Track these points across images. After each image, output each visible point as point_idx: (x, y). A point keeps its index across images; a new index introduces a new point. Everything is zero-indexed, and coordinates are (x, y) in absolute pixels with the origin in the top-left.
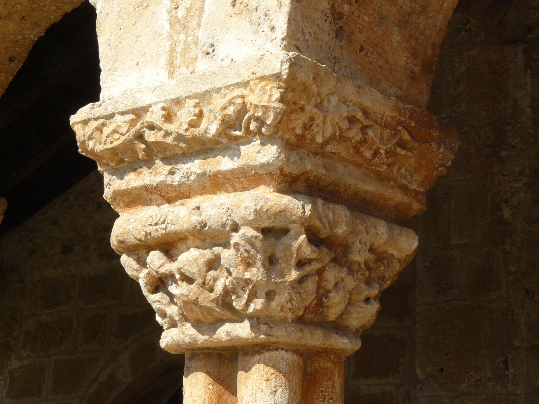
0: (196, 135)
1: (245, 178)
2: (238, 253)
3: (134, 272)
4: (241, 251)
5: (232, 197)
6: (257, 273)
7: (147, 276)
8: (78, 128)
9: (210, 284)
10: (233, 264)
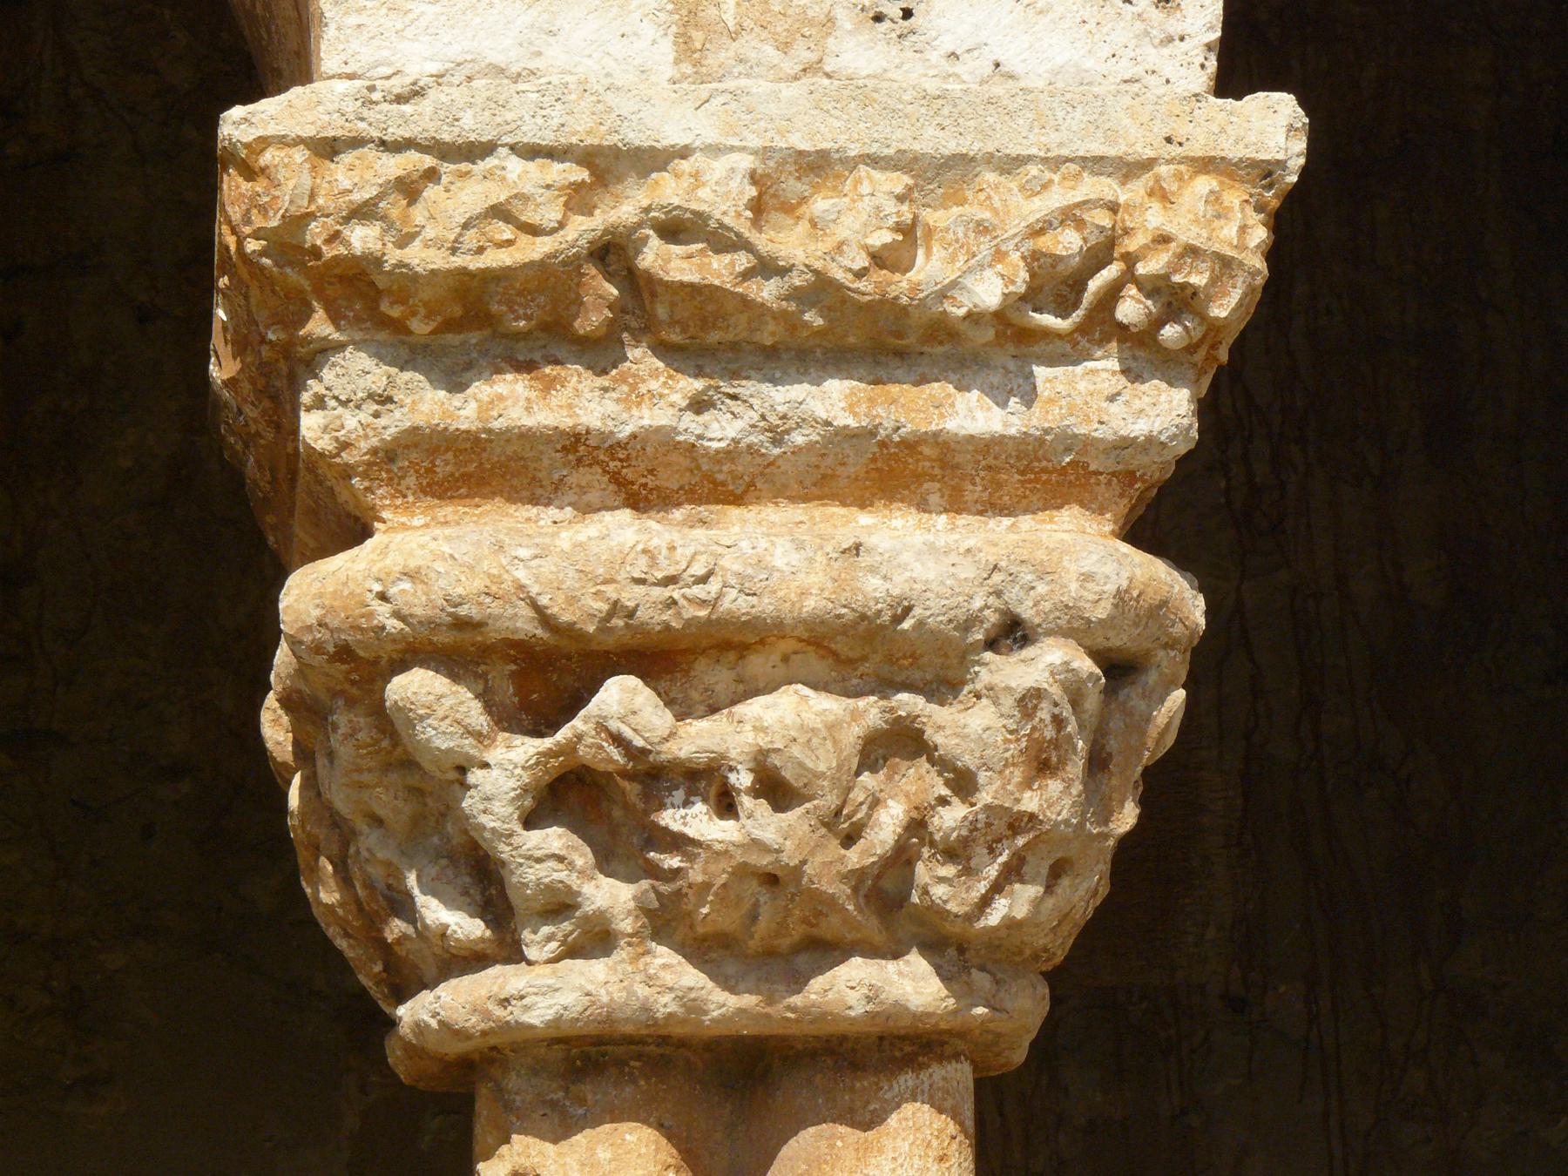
0: (896, 298)
1: (1022, 473)
2: (1026, 724)
3: (467, 742)
4: (1037, 719)
5: (940, 527)
6: (1060, 798)
7: (537, 764)
8: (286, 160)
9: (859, 816)
10: (995, 760)
